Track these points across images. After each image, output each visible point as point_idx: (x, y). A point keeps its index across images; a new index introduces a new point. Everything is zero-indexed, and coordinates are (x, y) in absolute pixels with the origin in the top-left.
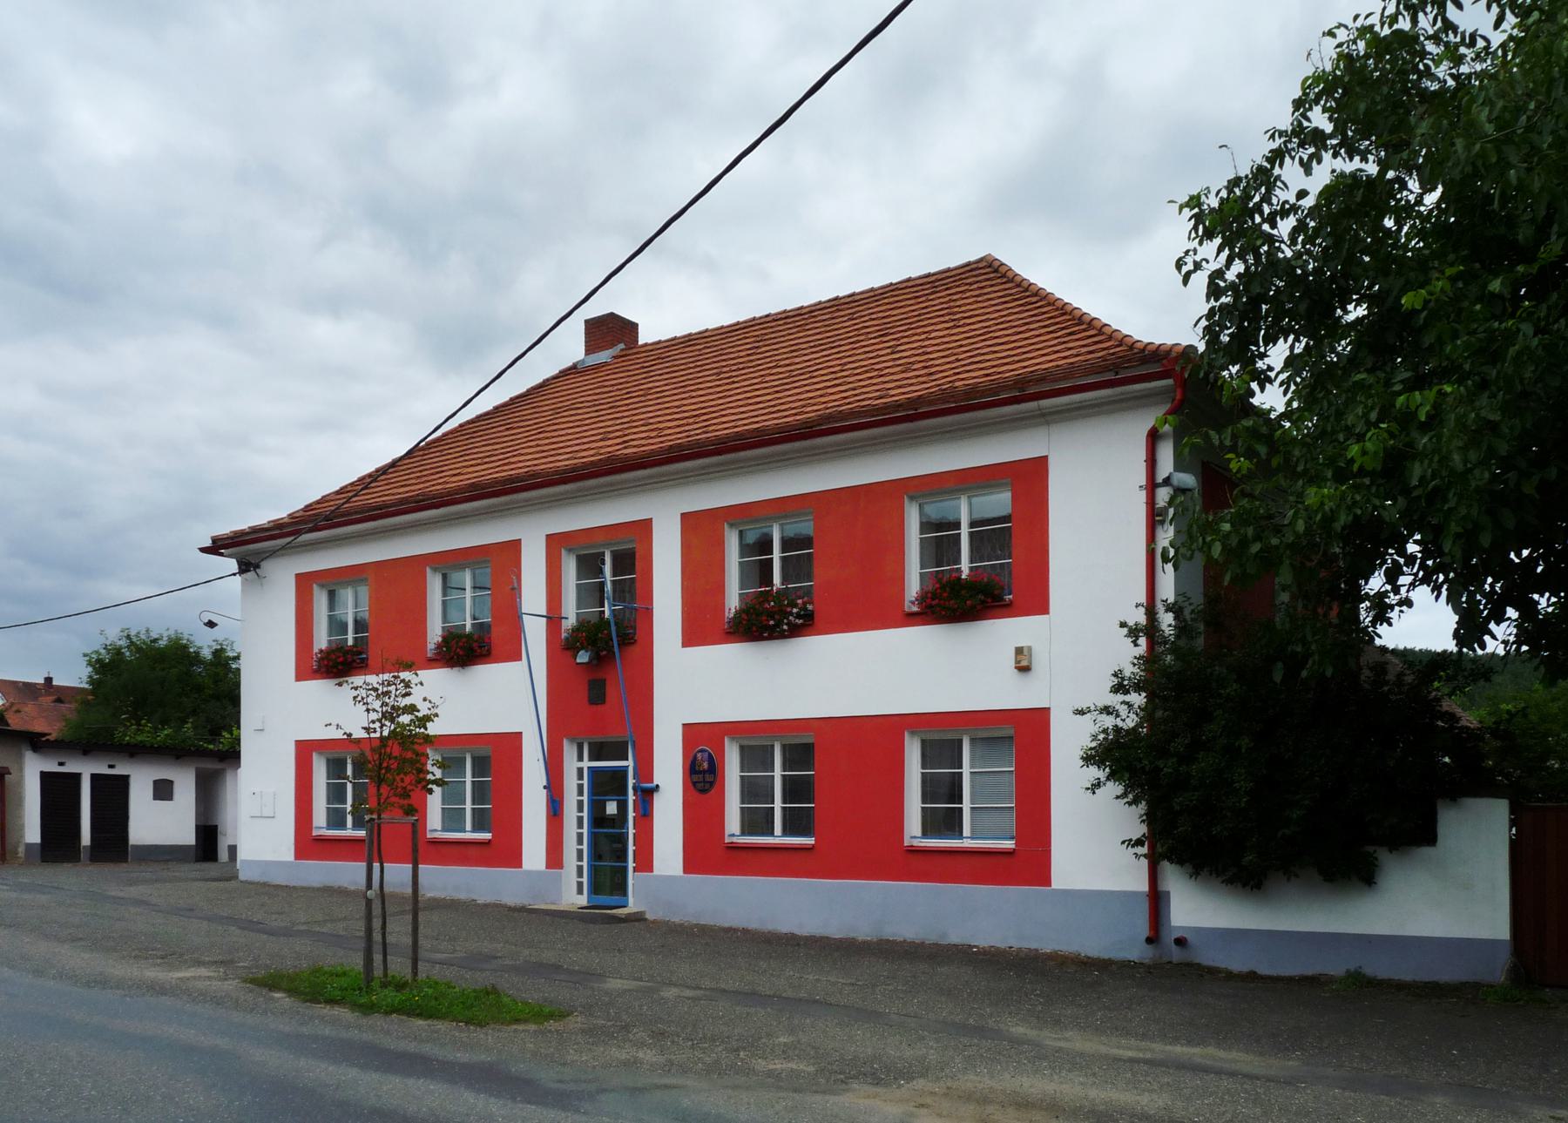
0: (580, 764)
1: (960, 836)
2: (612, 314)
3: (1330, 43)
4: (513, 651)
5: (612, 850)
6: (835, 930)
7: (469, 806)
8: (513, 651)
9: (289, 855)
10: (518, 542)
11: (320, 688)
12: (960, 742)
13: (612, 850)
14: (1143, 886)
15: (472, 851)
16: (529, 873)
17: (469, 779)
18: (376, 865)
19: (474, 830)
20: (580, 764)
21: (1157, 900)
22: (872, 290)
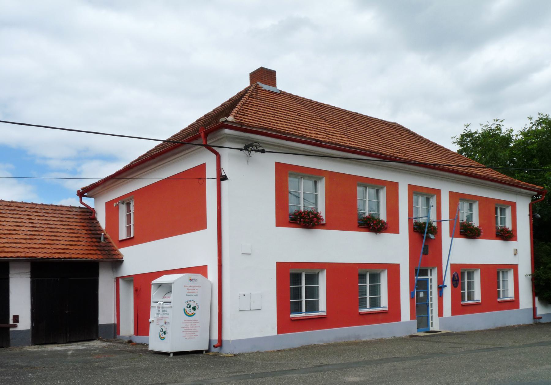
0: (431, 277)
1: (366, 307)
2: (262, 68)
3: (539, 116)
4: (396, 230)
5: (420, 308)
6: (492, 326)
7: (368, 296)
8: (396, 230)
9: (271, 329)
10: (205, 163)
11: (294, 233)
12: (365, 275)
13: (420, 308)
14: (531, 306)
15: (381, 316)
16: (522, 310)
17: (368, 284)
18: (215, 337)
19: (307, 311)
20: (431, 277)
21: (534, 309)
22: (304, 98)
